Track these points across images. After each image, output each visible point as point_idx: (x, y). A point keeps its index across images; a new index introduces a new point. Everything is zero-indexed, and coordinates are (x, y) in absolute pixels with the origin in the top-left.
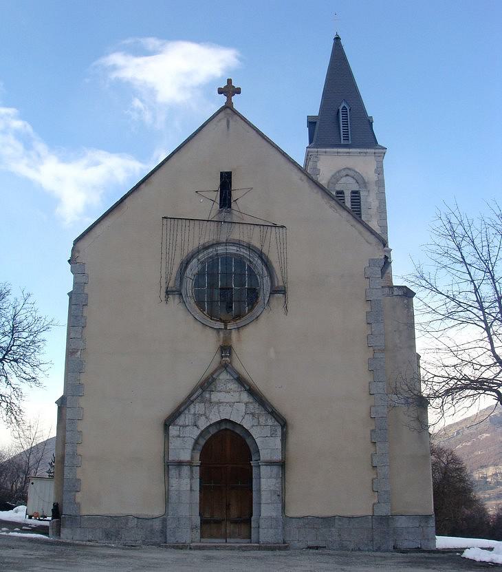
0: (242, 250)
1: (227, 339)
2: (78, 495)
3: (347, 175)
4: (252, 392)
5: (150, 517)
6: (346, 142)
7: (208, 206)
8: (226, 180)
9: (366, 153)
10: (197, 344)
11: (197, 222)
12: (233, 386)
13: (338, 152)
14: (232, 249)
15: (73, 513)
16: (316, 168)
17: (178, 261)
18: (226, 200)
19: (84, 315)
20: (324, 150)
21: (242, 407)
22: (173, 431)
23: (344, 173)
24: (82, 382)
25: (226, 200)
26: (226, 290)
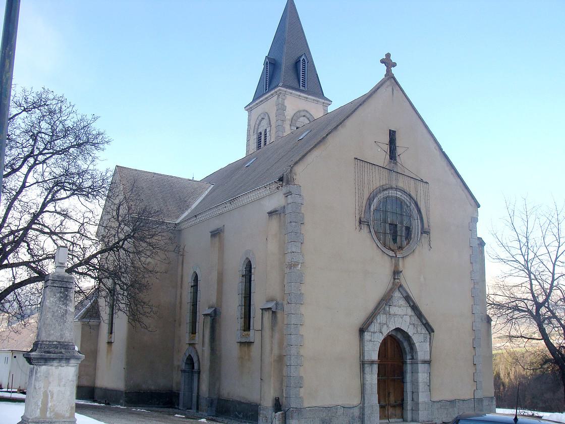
0: (404, 196)
1: (396, 265)
2: (302, 390)
3: (304, 116)
4: (415, 308)
5: (352, 406)
6: (303, 88)
7: (381, 156)
8: (392, 134)
9: (318, 101)
10: (380, 267)
11: (377, 167)
12: (402, 302)
13: (300, 96)
14: (399, 194)
15: (299, 407)
16: (284, 105)
17: (366, 196)
18: (393, 154)
19: (302, 232)
20: (291, 91)
21: (407, 319)
22: (367, 336)
23: (303, 114)
24: (303, 292)
25: (393, 154)
26: (393, 226)
